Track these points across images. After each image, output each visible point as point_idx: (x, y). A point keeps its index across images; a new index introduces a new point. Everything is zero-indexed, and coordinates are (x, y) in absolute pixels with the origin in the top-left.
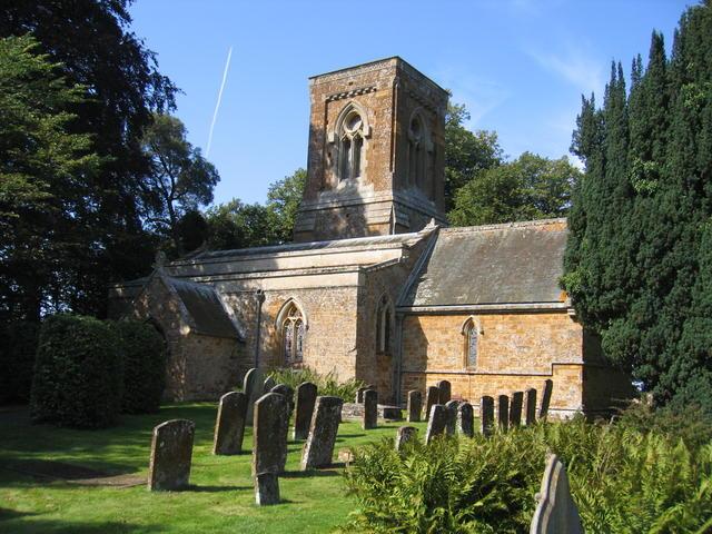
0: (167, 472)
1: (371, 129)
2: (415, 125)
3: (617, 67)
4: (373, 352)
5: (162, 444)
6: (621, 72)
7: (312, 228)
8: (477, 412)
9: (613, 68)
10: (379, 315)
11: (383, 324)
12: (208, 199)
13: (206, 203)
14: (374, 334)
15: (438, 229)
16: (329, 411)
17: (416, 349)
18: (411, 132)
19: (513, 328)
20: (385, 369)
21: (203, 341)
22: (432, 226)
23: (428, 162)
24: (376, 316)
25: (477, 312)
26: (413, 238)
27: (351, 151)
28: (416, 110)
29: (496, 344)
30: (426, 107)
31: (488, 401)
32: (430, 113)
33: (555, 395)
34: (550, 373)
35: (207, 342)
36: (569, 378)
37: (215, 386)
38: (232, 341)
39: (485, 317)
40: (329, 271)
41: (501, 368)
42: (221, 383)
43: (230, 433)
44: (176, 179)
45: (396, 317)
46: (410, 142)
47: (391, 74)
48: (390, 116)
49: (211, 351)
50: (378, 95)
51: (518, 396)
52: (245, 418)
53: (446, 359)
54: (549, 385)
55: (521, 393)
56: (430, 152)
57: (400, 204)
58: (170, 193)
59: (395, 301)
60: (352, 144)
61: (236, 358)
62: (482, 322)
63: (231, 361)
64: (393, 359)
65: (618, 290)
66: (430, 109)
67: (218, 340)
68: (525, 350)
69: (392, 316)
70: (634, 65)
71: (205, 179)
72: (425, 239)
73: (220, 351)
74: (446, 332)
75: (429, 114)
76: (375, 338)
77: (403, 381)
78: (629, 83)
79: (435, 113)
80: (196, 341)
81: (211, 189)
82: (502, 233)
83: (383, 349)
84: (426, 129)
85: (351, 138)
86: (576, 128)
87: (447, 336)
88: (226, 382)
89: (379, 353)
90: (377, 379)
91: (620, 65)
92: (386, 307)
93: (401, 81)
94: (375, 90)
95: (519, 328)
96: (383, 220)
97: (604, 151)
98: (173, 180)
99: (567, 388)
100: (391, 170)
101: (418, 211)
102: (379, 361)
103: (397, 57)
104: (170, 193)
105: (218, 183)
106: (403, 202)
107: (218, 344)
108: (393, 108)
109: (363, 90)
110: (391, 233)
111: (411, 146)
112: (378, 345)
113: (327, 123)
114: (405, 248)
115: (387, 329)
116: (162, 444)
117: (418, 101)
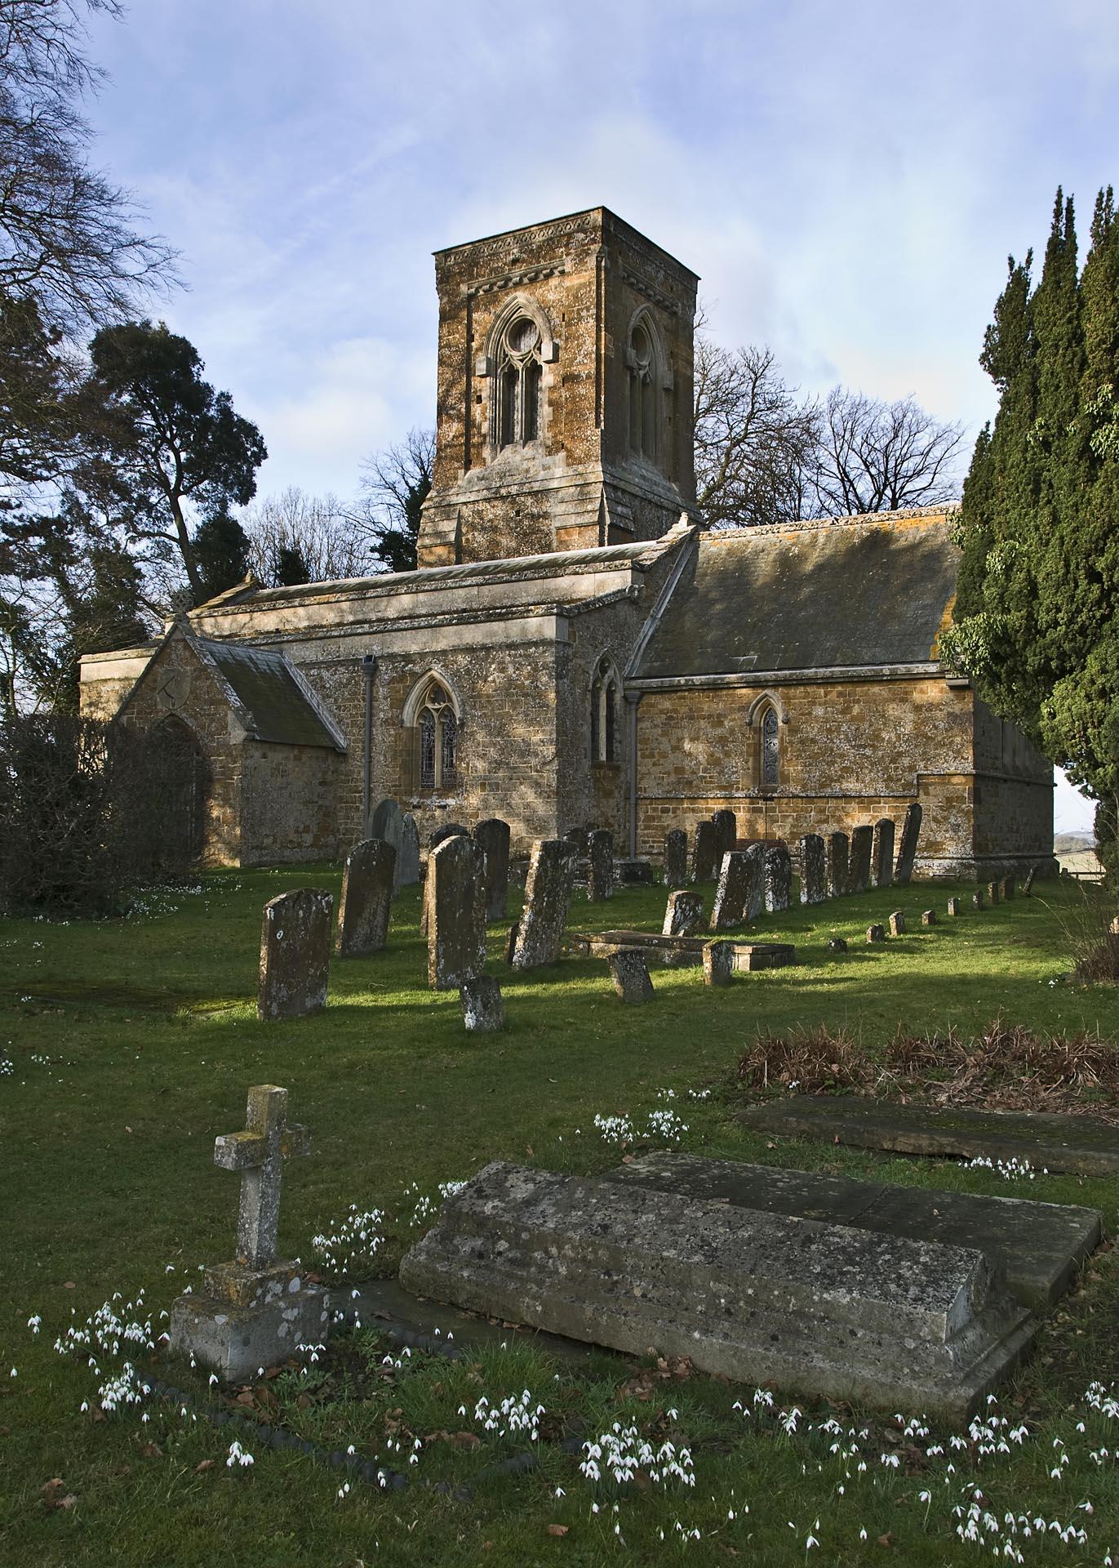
0: (289, 986)
1: (556, 348)
2: (639, 338)
3: (1064, 204)
4: (586, 763)
5: (280, 935)
6: (1070, 211)
7: (50, 583)
8: (798, 867)
9: (1058, 203)
10: (595, 694)
11: (603, 712)
12: (246, 491)
13: (244, 500)
14: (586, 729)
15: (695, 532)
16: (556, 866)
17: (664, 755)
18: (631, 352)
19: (844, 712)
20: (609, 794)
21: (270, 754)
22: (682, 527)
23: (665, 407)
24: (589, 696)
25: (777, 684)
26: (650, 550)
27: (519, 389)
28: (638, 310)
29: (813, 741)
30: (657, 303)
31: (814, 843)
32: (665, 315)
33: (926, 830)
34: (913, 792)
35: (277, 756)
36: (949, 800)
37: (292, 836)
38: (322, 754)
39: (792, 691)
40: (466, 617)
41: (823, 786)
42: (307, 830)
43: (366, 914)
44: (183, 455)
45: (625, 697)
46: (631, 369)
47: (594, 241)
48: (592, 322)
49: (284, 774)
50: (568, 283)
51: (864, 831)
52: (390, 887)
53: (721, 772)
54: (916, 810)
55: (870, 829)
56: (667, 390)
57: (615, 488)
58: (173, 479)
59: (621, 669)
60: (522, 375)
61: (331, 783)
62: (787, 700)
63: (321, 789)
64: (622, 776)
65: (1062, 629)
66: (666, 308)
67: (296, 752)
68: (868, 752)
69: (618, 697)
70: (1100, 200)
71: (240, 453)
72: (673, 551)
73: (300, 771)
74: (720, 724)
75: (663, 317)
76: (589, 735)
77: (642, 816)
78: (1085, 244)
79: (675, 313)
80: (257, 754)
81: (251, 474)
82: (815, 537)
83: (603, 758)
84: (658, 346)
85: (519, 366)
86: (994, 323)
87: (719, 731)
88: (314, 828)
89: (596, 765)
90: (594, 811)
91: (1070, 201)
92: (606, 680)
93: (609, 253)
94: (562, 272)
95: (856, 710)
96: (587, 519)
97: (1036, 371)
98: (178, 458)
99: (946, 818)
100: (597, 425)
101: (650, 502)
102: (597, 780)
103: (604, 208)
104: (173, 479)
105: (263, 462)
106: (622, 485)
107: (297, 758)
108: (598, 306)
109: (537, 274)
110: (601, 544)
111: (633, 378)
112: (595, 750)
113: (471, 338)
114: (638, 568)
115: (610, 721)
116: (280, 935)
117: (645, 285)
